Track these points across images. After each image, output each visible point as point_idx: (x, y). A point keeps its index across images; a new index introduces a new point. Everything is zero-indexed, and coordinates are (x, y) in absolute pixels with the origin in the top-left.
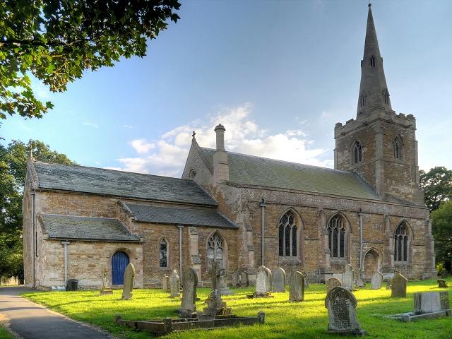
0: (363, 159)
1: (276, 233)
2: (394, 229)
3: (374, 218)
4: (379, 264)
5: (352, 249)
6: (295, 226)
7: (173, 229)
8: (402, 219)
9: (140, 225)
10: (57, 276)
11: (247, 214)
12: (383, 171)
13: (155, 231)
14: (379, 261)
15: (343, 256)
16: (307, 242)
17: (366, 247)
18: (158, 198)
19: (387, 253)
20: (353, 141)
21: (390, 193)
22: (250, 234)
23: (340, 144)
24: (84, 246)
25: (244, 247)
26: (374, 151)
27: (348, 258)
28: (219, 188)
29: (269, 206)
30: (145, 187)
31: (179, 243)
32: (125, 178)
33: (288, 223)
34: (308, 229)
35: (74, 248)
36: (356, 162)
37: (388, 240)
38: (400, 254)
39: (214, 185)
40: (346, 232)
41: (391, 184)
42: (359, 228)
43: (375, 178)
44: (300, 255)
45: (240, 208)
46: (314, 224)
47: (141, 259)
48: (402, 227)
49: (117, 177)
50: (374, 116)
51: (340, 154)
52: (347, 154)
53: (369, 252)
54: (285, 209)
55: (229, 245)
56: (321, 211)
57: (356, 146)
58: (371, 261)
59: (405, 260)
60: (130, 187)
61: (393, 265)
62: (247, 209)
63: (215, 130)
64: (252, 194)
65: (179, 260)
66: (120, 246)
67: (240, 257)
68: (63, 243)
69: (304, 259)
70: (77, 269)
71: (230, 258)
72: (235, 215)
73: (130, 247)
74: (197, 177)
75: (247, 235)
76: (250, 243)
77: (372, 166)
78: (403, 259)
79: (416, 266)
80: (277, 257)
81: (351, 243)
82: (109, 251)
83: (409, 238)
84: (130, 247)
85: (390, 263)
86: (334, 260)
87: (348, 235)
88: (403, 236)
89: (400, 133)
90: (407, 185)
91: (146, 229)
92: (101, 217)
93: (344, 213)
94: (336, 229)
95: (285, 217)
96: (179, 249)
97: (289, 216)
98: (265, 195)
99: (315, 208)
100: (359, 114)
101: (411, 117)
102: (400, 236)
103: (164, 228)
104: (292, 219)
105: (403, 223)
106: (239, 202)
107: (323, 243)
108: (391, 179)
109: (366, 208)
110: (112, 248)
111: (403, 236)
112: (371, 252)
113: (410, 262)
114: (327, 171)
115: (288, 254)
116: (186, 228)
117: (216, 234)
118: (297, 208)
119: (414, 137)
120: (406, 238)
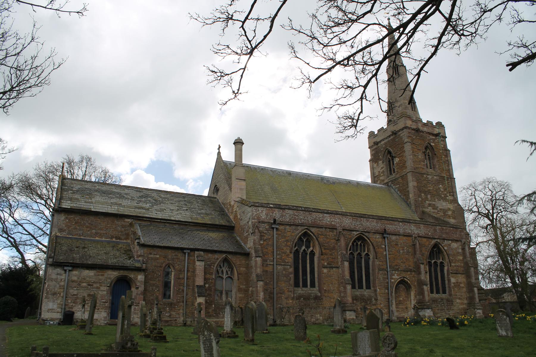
0: (396, 170)
1: (290, 259)
2: (427, 254)
3: (402, 240)
4: (413, 297)
5: (378, 277)
6: (312, 251)
7: (180, 255)
8: (433, 242)
9: (146, 250)
10: (55, 307)
11: (257, 237)
12: (415, 184)
13: (160, 256)
14: (413, 294)
15: (370, 288)
16: (325, 271)
17: (396, 277)
18: (172, 218)
19: (421, 284)
20: (384, 150)
21: (426, 210)
22: (259, 259)
23: (373, 152)
24: (87, 273)
25: (254, 276)
26: (405, 162)
27: (376, 291)
28: (235, 207)
29: (281, 227)
30: (163, 206)
31: (184, 271)
32: (146, 196)
33: (304, 248)
34: (326, 254)
35: (75, 274)
36: (391, 174)
37: (419, 268)
38: (437, 284)
39: (232, 203)
40: (371, 257)
41: (427, 199)
42: (385, 253)
43: (408, 191)
44: (319, 286)
45: (251, 230)
46: (334, 248)
47: (142, 288)
48: (436, 251)
49: (139, 194)
50: (401, 125)
51: (375, 165)
52: (381, 166)
53: (399, 283)
54: (300, 231)
55: (238, 274)
56: (340, 232)
57: (389, 156)
58: (403, 294)
59: (444, 292)
60: (148, 206)
61: (427, 298)
62: (257, 231)
63: (234, 143)
64: (263, 214)
65: (183, 290)
66: (122, 273)
67: (251, 289)
68: (65, 268)
69: (323, 292)
70: (76, 299)
71: (240, 290)
72: (247, 238)
73: (132, 275)
74: (219, 193)
75: (256, 261)
76: (259, 271)
77: (404, 177)
78: (441, 291)
79: (458, 301)
80: (291, 288)
81: (377, 270)
82: (110, 278)
83: (446, 264)
84: (132, 275)
85: (424, 296)
86: (358, 292)
87: (373, 261)
88: (439, 262)
89: (431, 143)
90: (445, 199)
91: (151, 254)
92: (114, 240)
93: (367, 234)
94: (359, 254)
95: (300, 239)
96: (184, 278)
97: (306, 238)
98: (277, 214)
99: (333, 228)
100: (389, 122)
101: (440, 125)
102: (435, 262)
103: (170, 254)
104: (310, 242)
105: (436, 246)
106: (250, 223)
107: (343, 272)
108: (426, 193)
109: (390, 227)
110: (113, 274)
111: (439, 262)
112: (402, 282)
113: (450, 295)
114: (358, 185)
115: (305, 285)
116: (192, 253)
117: (225, 260)
118: (313, 230)
119: (445, 145)
120: (442, 265)
